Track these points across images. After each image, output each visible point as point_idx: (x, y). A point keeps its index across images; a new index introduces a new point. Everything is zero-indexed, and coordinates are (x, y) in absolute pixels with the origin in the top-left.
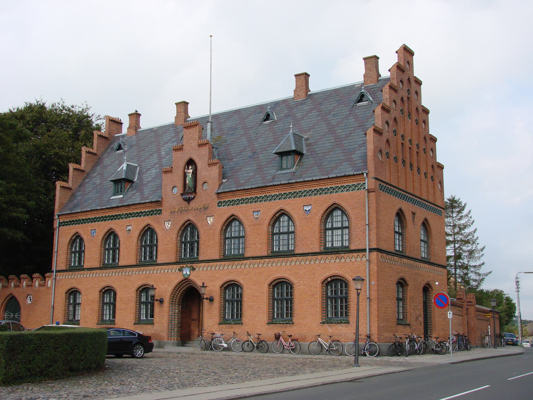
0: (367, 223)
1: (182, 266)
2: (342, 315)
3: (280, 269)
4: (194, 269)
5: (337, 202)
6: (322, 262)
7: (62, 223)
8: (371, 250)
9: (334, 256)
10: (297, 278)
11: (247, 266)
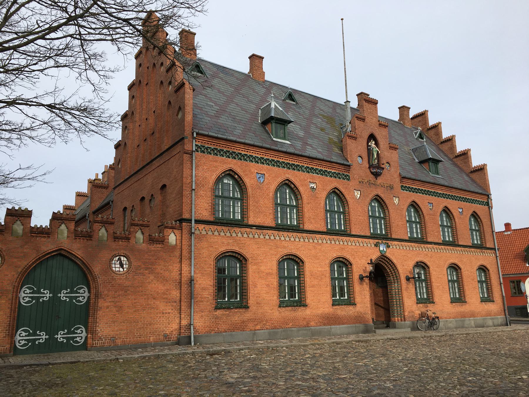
1: (377, 241)
3: (292, 244)
8: (190, 221)
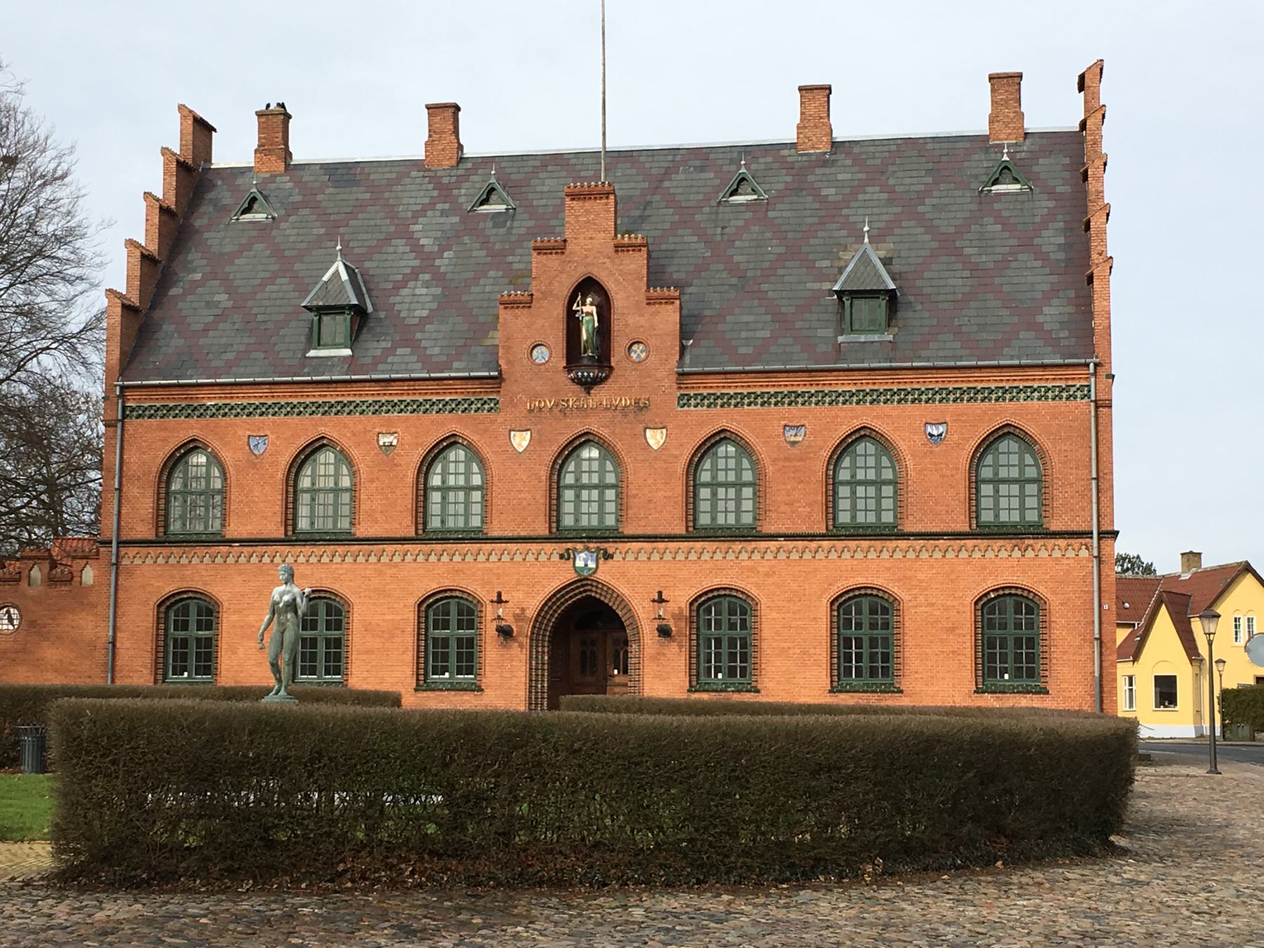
0: (1094, 475)
1: (569, 545)
2: (859, 674)
4: (607, 556)
5: (1014, 421)
6: (977, 555)
7: (133, 410)
9: (1008, 544)
10: (909, 590)
11: (769, 556)
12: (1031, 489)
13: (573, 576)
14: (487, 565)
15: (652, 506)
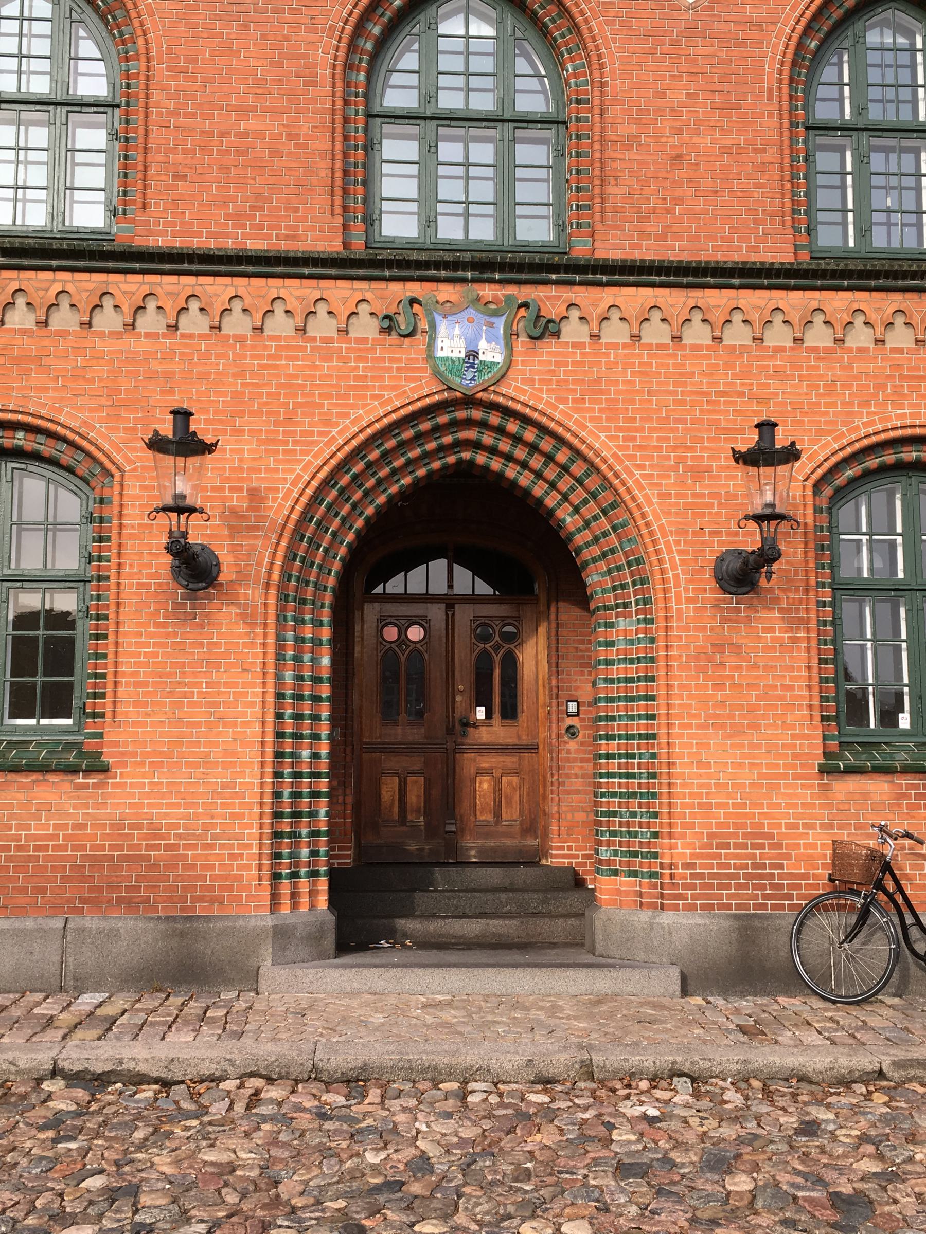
4: (545, 329)
12: (533, 153)
13: (420, 390)
14: (130, 343)
15: (681, 174)
